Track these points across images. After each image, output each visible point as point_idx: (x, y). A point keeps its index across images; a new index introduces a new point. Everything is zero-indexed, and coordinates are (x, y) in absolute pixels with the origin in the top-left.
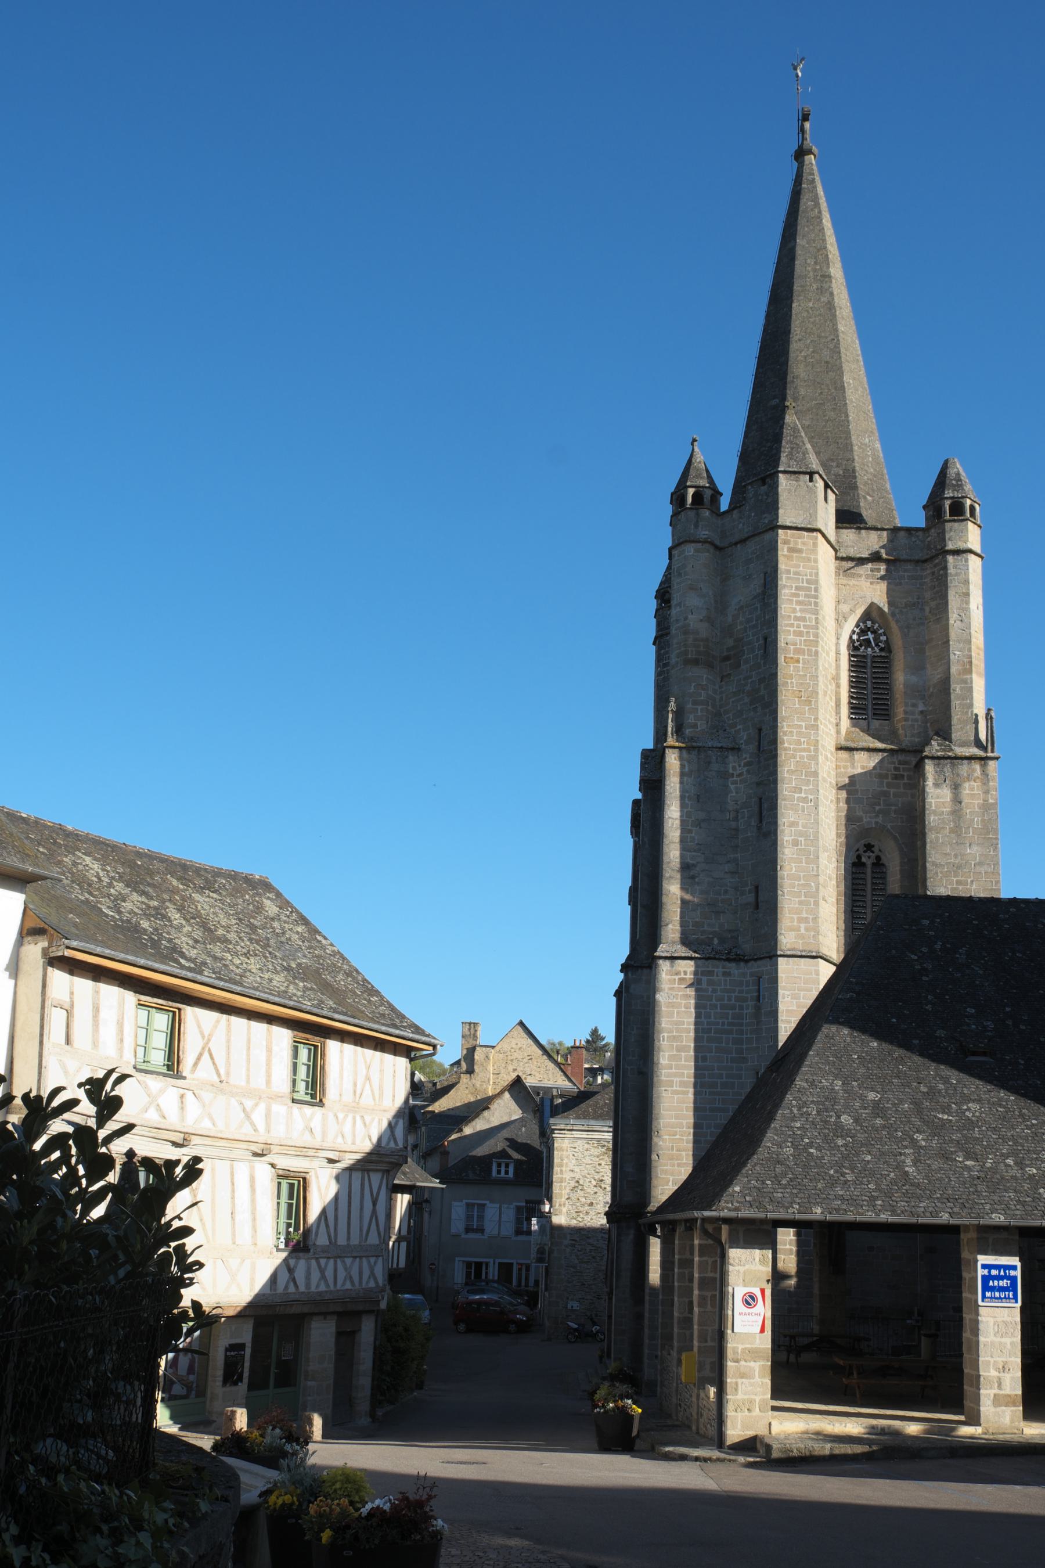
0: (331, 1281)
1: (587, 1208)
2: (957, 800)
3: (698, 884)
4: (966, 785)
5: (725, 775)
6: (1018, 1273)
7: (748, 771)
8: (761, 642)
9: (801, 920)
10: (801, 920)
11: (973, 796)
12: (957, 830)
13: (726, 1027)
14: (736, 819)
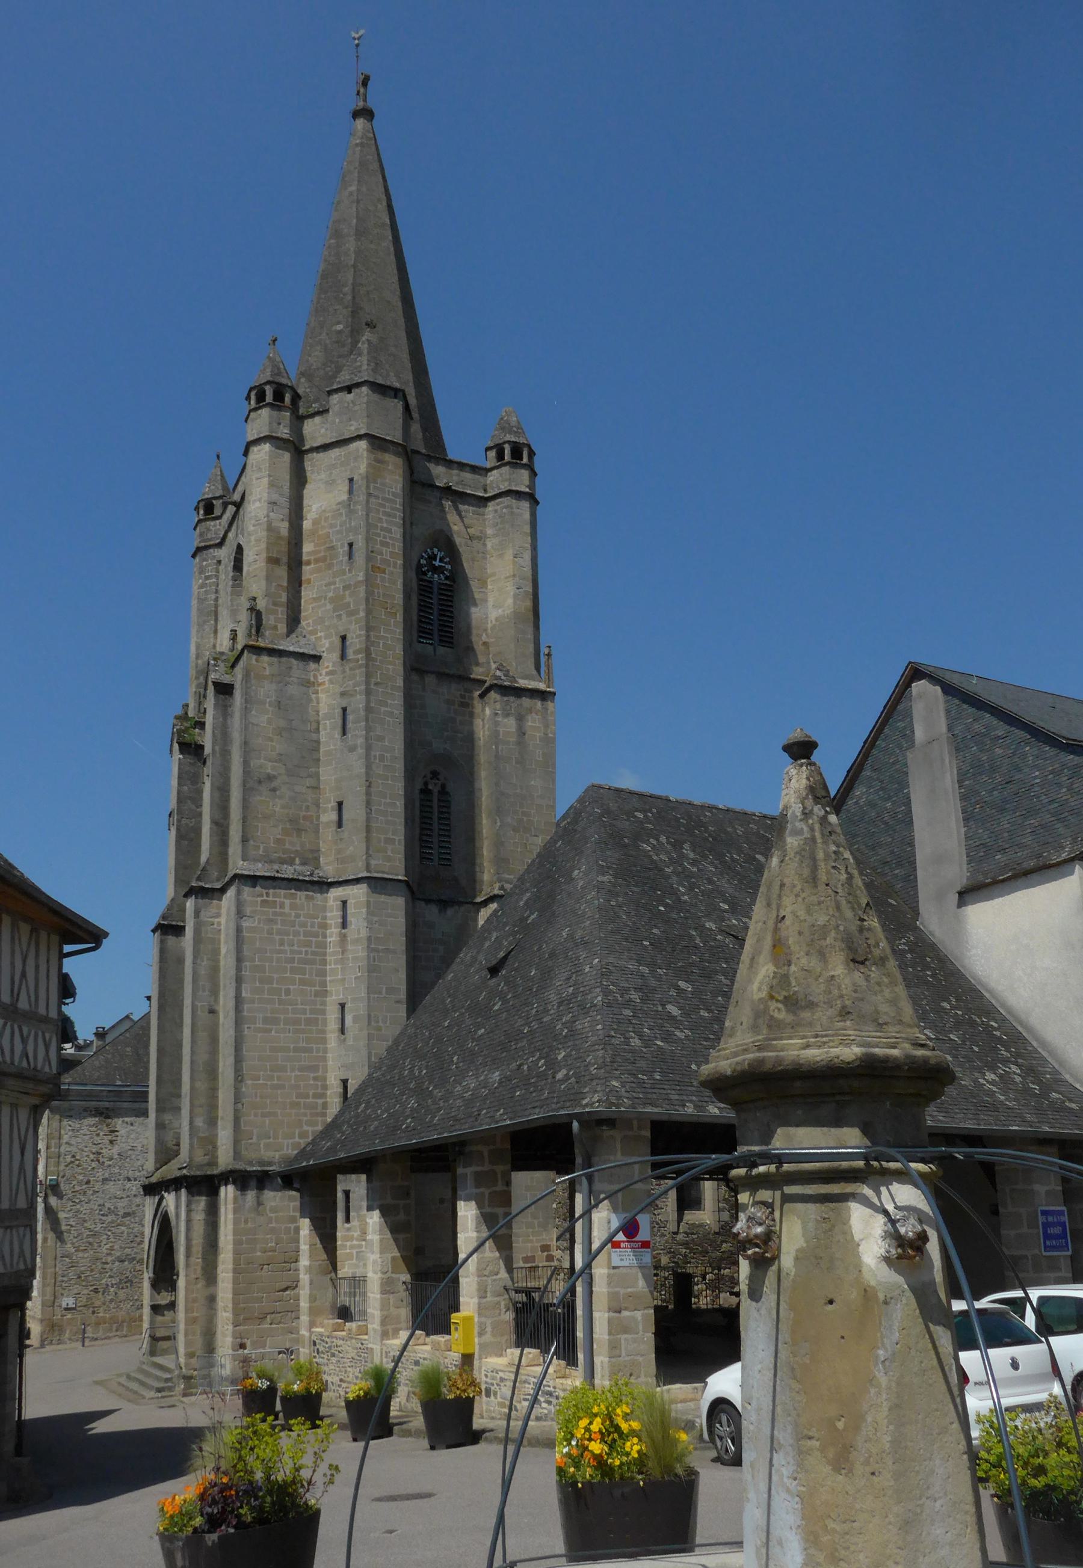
2: (522, 733)
3: (280, 798)
4: (529, 717)
6: (1065, 1218)
7: (331, 682)
8: (346, 548)
13: (309, 956)
14: (317, 731)
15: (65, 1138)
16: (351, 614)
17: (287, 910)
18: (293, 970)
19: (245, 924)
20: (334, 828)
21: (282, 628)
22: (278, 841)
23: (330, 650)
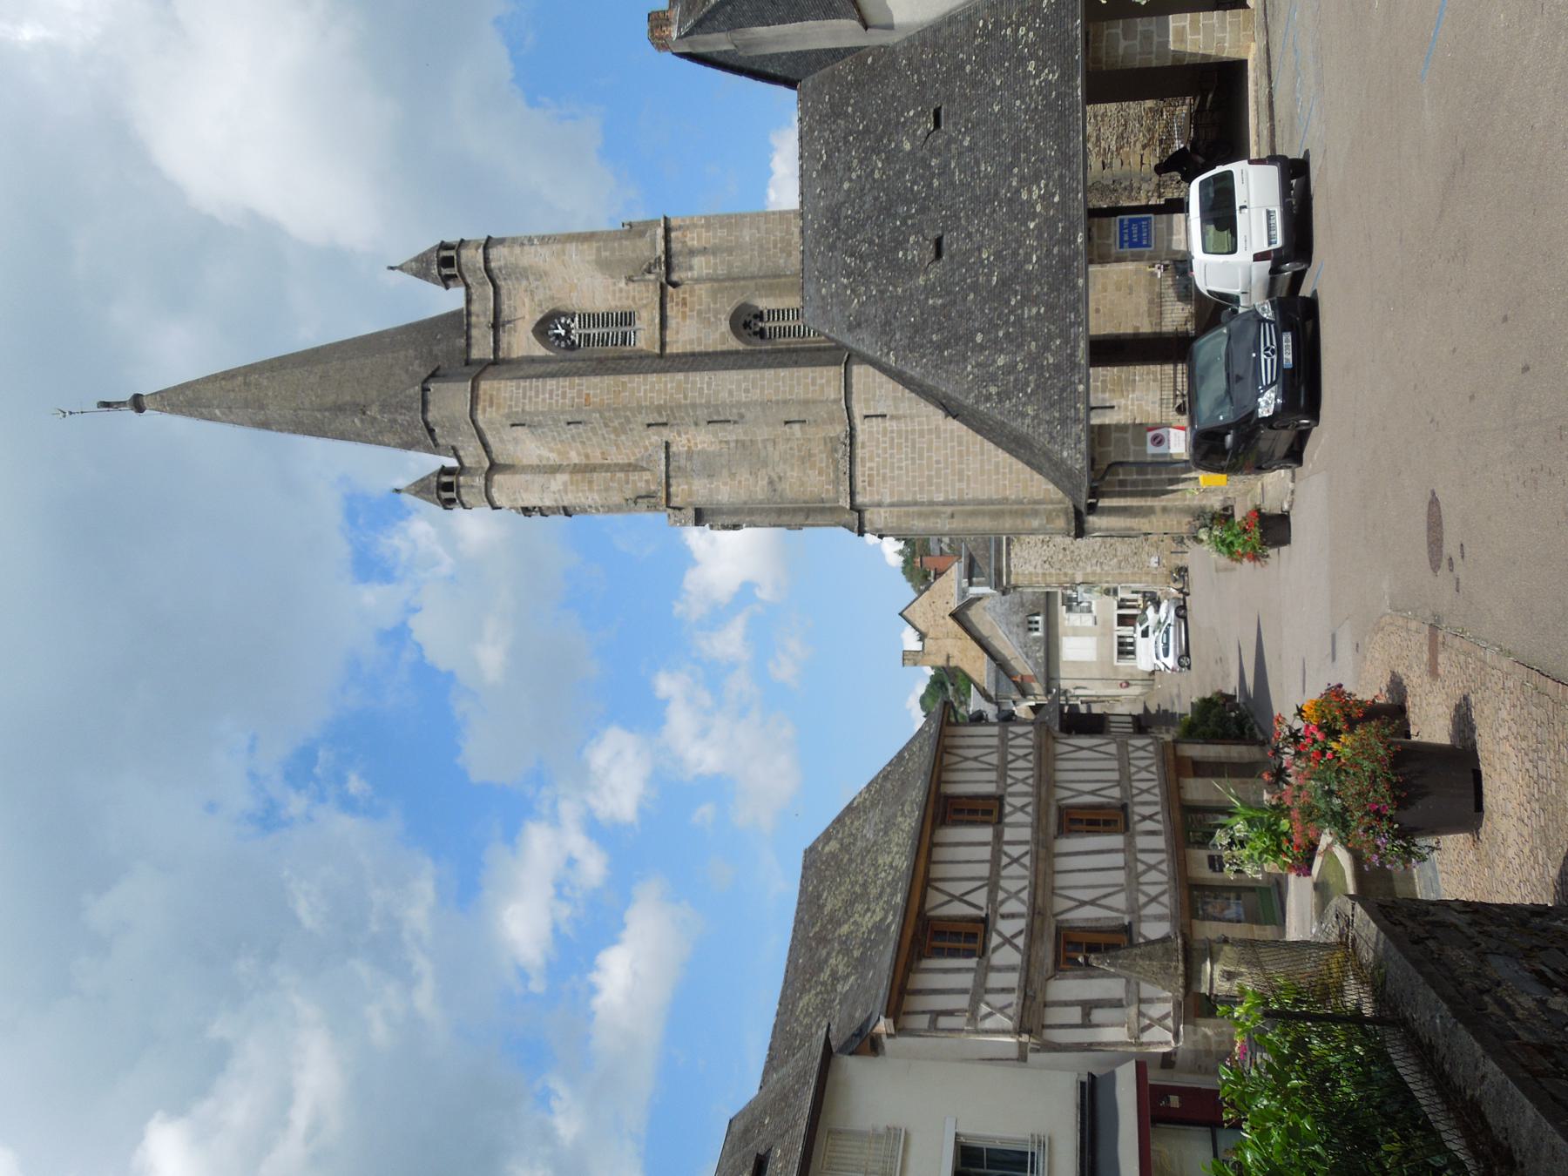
0: (1148, 762)
2: (704, 251)
5: (690, 454)
9: (814, 383)
10: (814, 383)
11: (699, 238)
12: (730, 251)
14: (727, 442)
15: (1031, 569)
16: (628, 421)
17: (874, 465)
18: (921, 457)
19: (888, 500)
20: (806, 427)
21: (647, 476)
22: (820, 474)
23: (660, 435)
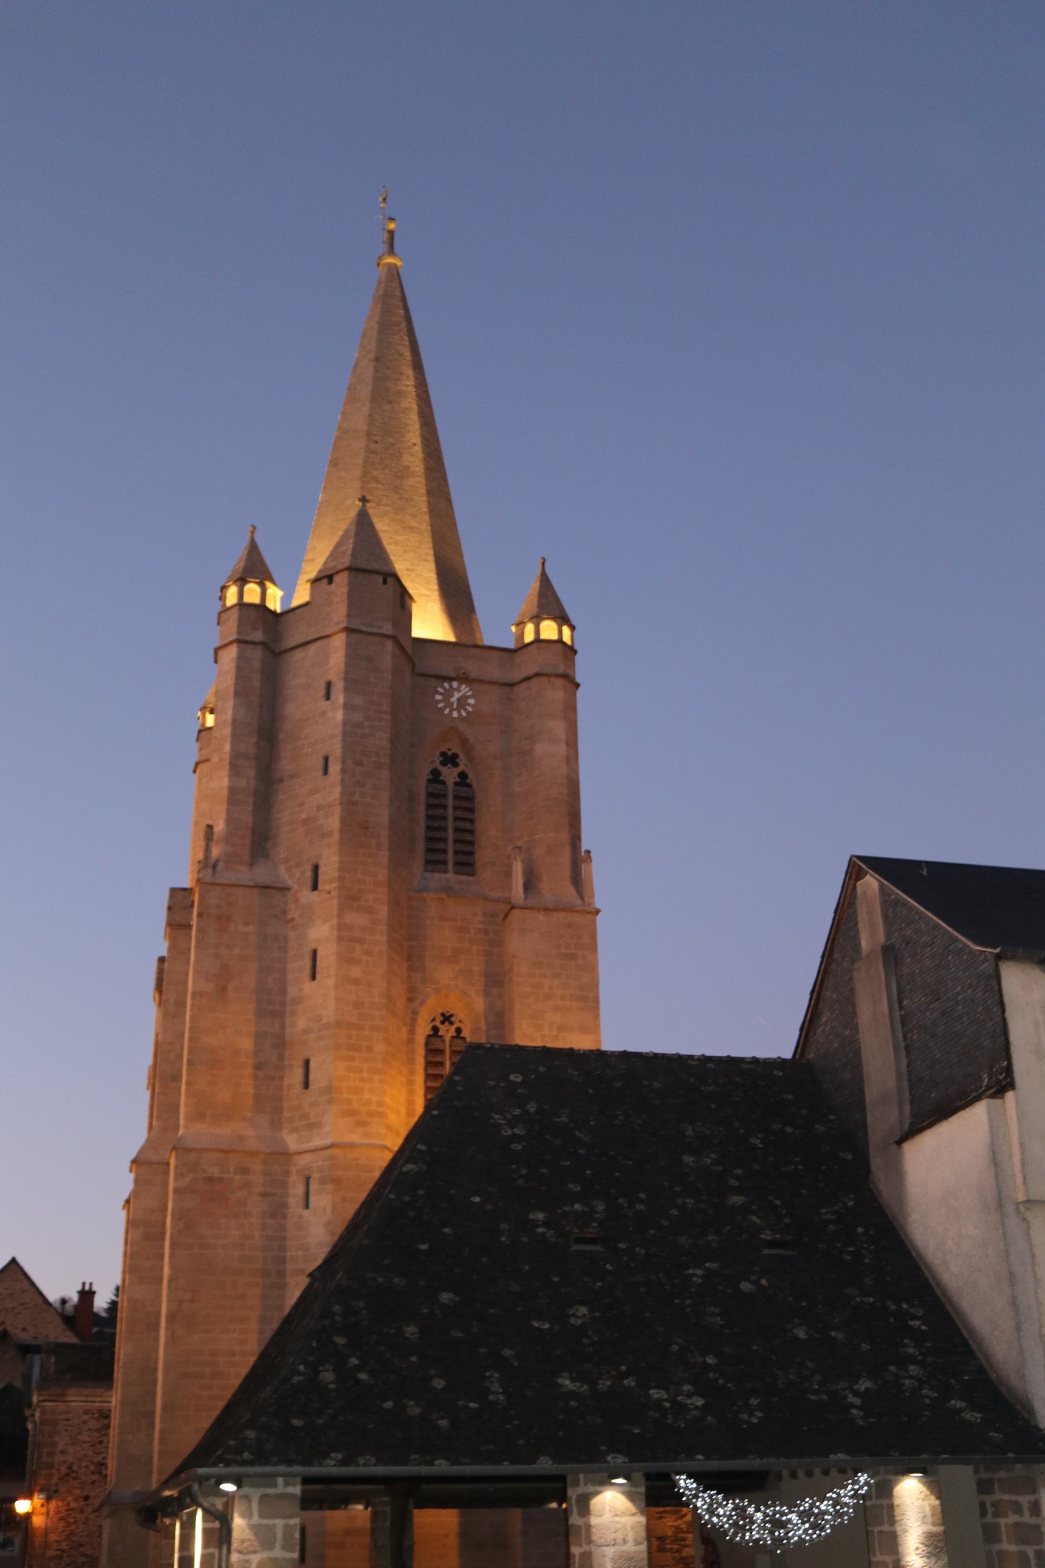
1: (82, 1503)
